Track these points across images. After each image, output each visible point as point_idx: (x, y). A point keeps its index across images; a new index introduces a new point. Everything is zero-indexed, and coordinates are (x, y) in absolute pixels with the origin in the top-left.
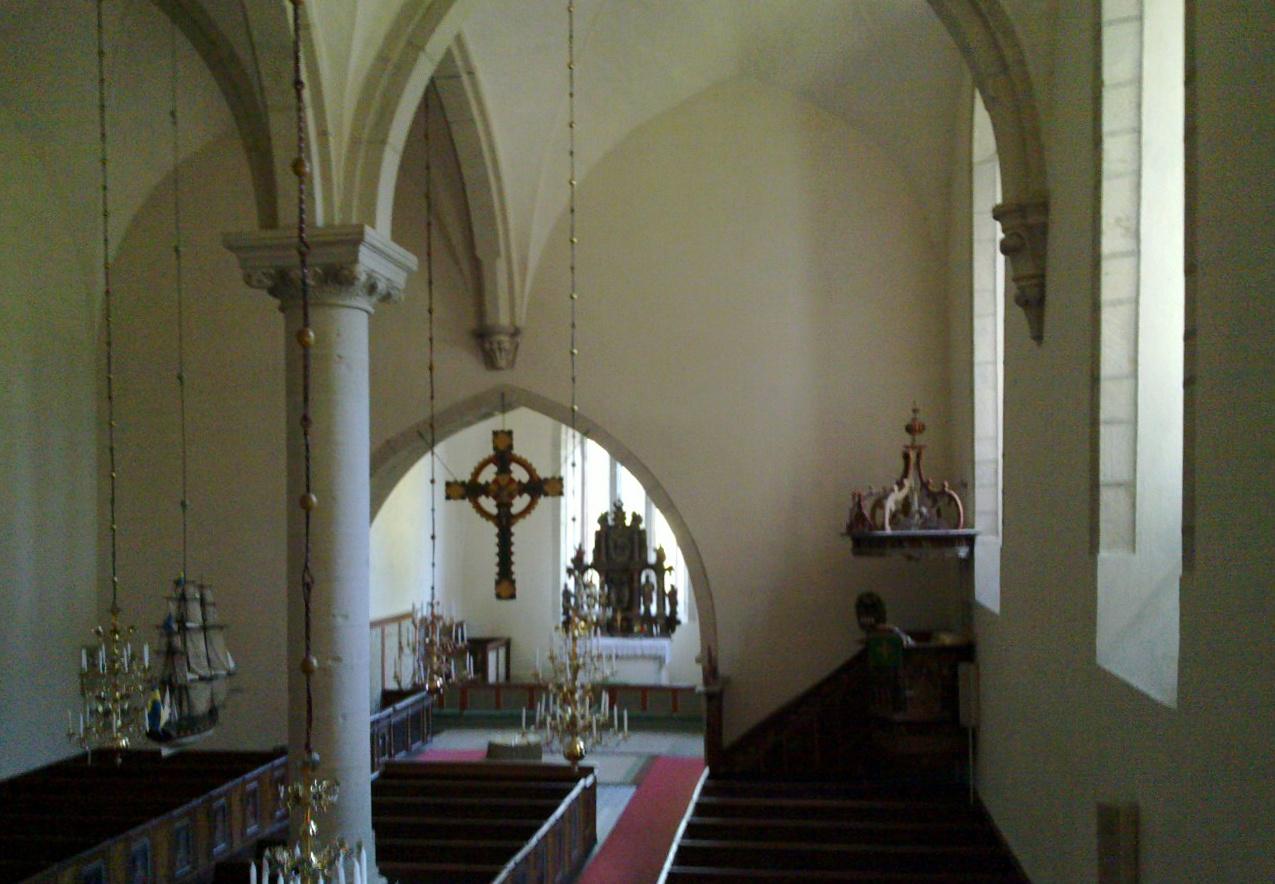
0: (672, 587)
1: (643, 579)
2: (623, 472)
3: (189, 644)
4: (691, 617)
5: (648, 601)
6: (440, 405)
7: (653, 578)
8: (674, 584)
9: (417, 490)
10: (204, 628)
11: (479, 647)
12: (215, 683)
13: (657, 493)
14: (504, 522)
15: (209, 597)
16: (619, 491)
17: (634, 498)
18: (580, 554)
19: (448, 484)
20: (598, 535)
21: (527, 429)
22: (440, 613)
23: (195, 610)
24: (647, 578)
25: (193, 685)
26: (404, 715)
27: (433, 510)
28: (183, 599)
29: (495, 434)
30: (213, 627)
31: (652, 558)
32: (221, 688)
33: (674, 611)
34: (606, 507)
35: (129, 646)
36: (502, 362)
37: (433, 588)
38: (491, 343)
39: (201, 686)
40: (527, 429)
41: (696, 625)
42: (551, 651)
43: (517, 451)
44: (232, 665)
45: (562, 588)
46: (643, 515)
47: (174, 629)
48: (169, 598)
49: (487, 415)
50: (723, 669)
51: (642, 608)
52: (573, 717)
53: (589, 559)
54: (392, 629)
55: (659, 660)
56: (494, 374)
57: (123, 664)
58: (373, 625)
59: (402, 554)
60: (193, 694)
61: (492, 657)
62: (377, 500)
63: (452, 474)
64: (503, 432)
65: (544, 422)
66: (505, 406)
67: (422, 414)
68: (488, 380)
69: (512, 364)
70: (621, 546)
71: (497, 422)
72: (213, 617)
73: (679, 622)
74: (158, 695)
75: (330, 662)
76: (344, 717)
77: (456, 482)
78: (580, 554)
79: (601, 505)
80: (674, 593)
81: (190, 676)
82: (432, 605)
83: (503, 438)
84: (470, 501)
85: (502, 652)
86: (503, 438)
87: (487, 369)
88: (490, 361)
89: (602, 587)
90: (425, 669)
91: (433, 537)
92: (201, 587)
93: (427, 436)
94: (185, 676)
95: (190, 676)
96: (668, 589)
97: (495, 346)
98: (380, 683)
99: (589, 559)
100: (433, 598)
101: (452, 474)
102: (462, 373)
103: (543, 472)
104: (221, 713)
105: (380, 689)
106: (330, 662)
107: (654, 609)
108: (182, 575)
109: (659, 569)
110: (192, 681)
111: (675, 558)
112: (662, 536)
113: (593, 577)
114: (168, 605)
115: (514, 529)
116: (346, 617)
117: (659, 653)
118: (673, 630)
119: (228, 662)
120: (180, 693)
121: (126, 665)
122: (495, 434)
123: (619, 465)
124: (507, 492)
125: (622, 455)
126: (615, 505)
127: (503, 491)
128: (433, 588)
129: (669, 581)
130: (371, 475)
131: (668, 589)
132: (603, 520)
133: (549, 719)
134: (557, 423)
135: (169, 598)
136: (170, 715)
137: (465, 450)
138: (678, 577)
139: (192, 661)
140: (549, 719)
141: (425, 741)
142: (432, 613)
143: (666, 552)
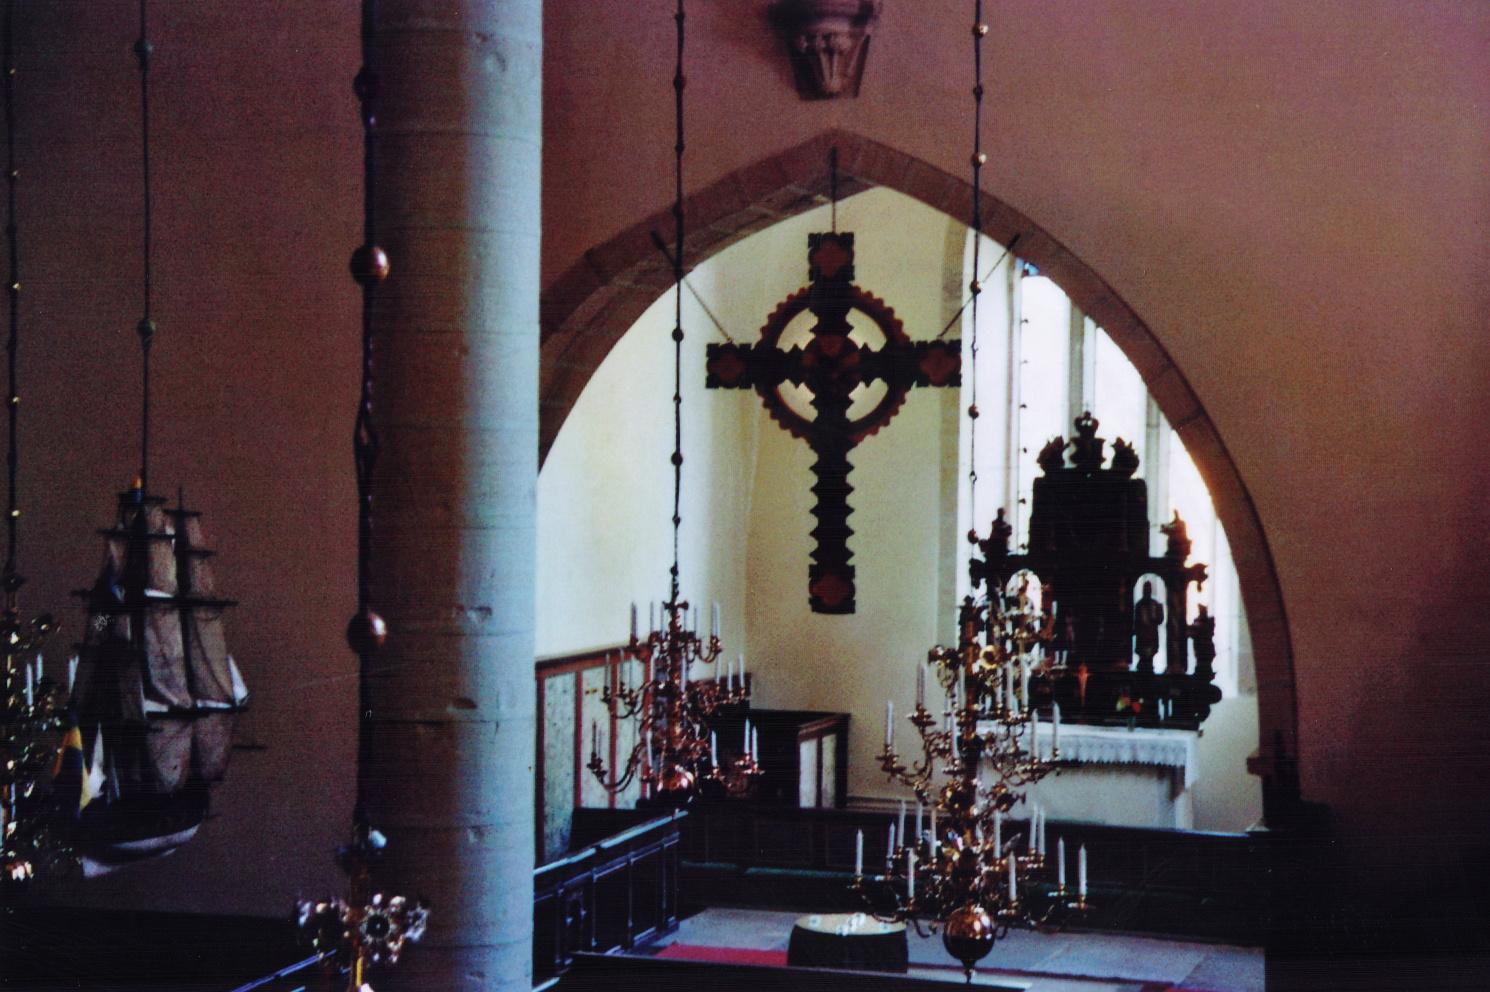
0: (1203, 610)
1: (1138, 594)
2: (1102, 347)
3: (150, 634)
4: (1242, 685)
5: (1148, 648)
6: (701, 175)
7: (1160, 594)
8: (1204, 604)
9: (649, 365)
10: (185, 603)
11: (783, 731)
12: (206, 724)
13: (1177, 397)
14: (832, 442)
15: (196, 536)
16: (1087, 397)
17: (1122, 405)
18: (1001, 529)
19: (713, 351)
20: (1038, 485)
21: (896, 241)
22: (690, 628)
23: (166, 566)
24: (1148, 587)
25: (156, 725)
26: (618, 865)
27: (678, 399)
28: (139, 542)
29: (815, 241)
30: (201, 603)
31: (1158, 546)
32: (216, 739)
33: (1205, 670)
34: (1059, 427)
35: (40, 660)
36: (835, 83)
37: (674, 571)
38: (811, 38)
39: (170, 728)
40: (896, 241)
41: (1252, 703)
42: (919, 708)
43: (865, 279)
44: (240, 692)
45: (960, 602)
46: (1139, 449)
47: (121, 592)
48: (111, 534)
49: (799, 204)
50: (1312, 784)
51: (1136, 659)
52: (967, 855)
53: (1019, 540)
54: (595, 678)
55: (1171, 776)
56: (819, 107)
57: (23, 699)
58: (546, 668)
59: (609, 516)
60: (156, 742)
61: (807, 750)
62: (558, 396)
63: (725, 334)
64: (831, 236)
65: (931, 222)
66: (838, 187)
67: (657, 199)
68: (808, 120)
69: (854, 86)
70: (1086, 499)
71: (818, 219)
72: (204, 579)
73: (1216, 695)
74: (77, 738)
75: (451, 709)
76: (479, 831)
77: (729, 346)
78: (1001, 529)
79: (1049, 424)
80: (1206, 624)
81: (150, 706)
82: (671, 607)
83: (832, 257)
84: (760, 393)
85: (829, 743)
86: (832, 257)
87: (802, 98)
88: (809, 84)
89: (1046, 608)
90: (656, 751)
91: (677, 459)
92: (180, 517)
93: (666, 249)
94: (139, 707)
95: (150, 706)
96: (1192, 616)
97: (821, 44)
98: (570, 796)
99: (1019, 540)
100: (675, 594)
101: (725, 334)
102: (749, 107)
103: (920, 328)
104: (217, 797)
105: (569, 808)
106: (451, 709)
107: (1160, 663)
108: (139, 484)
109: (1179, 572)
110: (153, 715)
111: (1210, 545)
112: (1180, 492)
113: (1032, 589)
114: (107, 546)
115: (852, 456)
116: (486, 611)
117: (1171, 760)
118: (1205, 714)
119: (231, 682)
120: (131, 749)
121: (30, 701)
122: (815, 241)
123: (1089, 323)
124: (834, 378)
125: (1098, 300)
126: (1078, 423)
127: (832, 367)
128: (674, 571)
129: (1195, 598)
130: (544, 338)
131: (1192, 616)
132: (1050, 456)
133: (913, 858)
134: (958, 225)
135: (111, 534)
136: (104, 787)
137: (749, 276)
138: (1219, 595)
139: (155, 673)
140: (913, 858)
141: (665, 929)
142: (673, 624)
143: (1190, 534)
